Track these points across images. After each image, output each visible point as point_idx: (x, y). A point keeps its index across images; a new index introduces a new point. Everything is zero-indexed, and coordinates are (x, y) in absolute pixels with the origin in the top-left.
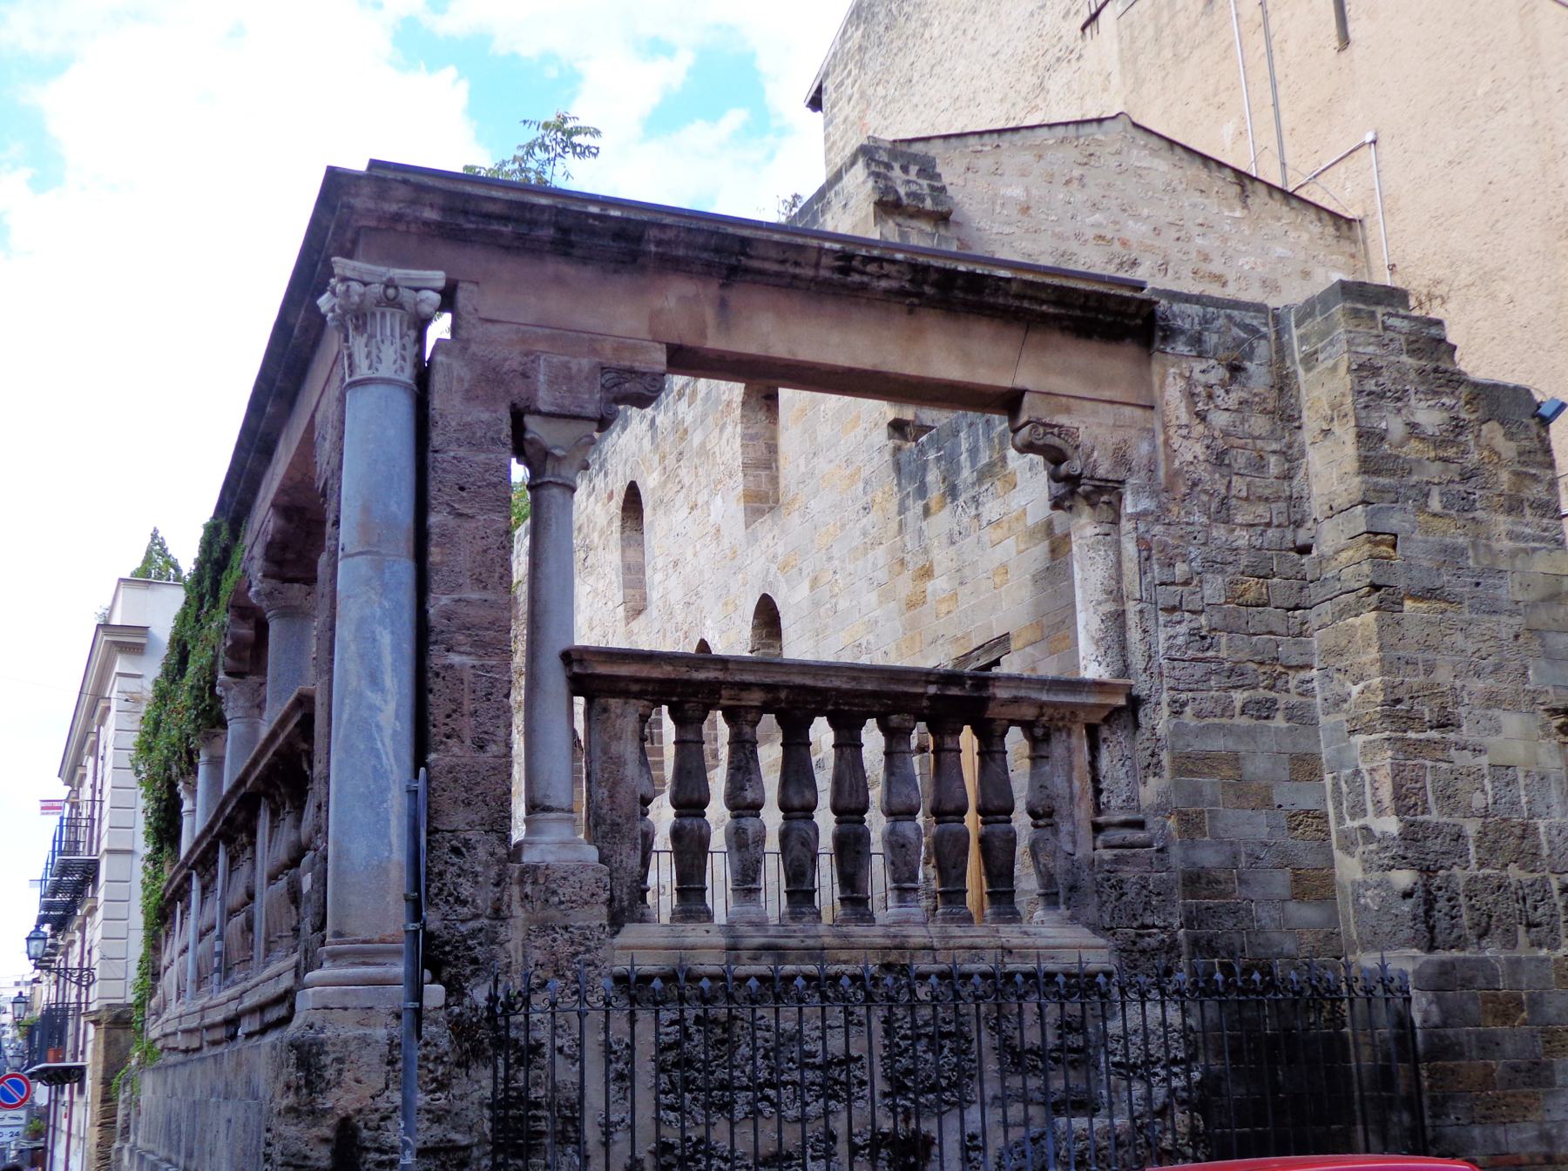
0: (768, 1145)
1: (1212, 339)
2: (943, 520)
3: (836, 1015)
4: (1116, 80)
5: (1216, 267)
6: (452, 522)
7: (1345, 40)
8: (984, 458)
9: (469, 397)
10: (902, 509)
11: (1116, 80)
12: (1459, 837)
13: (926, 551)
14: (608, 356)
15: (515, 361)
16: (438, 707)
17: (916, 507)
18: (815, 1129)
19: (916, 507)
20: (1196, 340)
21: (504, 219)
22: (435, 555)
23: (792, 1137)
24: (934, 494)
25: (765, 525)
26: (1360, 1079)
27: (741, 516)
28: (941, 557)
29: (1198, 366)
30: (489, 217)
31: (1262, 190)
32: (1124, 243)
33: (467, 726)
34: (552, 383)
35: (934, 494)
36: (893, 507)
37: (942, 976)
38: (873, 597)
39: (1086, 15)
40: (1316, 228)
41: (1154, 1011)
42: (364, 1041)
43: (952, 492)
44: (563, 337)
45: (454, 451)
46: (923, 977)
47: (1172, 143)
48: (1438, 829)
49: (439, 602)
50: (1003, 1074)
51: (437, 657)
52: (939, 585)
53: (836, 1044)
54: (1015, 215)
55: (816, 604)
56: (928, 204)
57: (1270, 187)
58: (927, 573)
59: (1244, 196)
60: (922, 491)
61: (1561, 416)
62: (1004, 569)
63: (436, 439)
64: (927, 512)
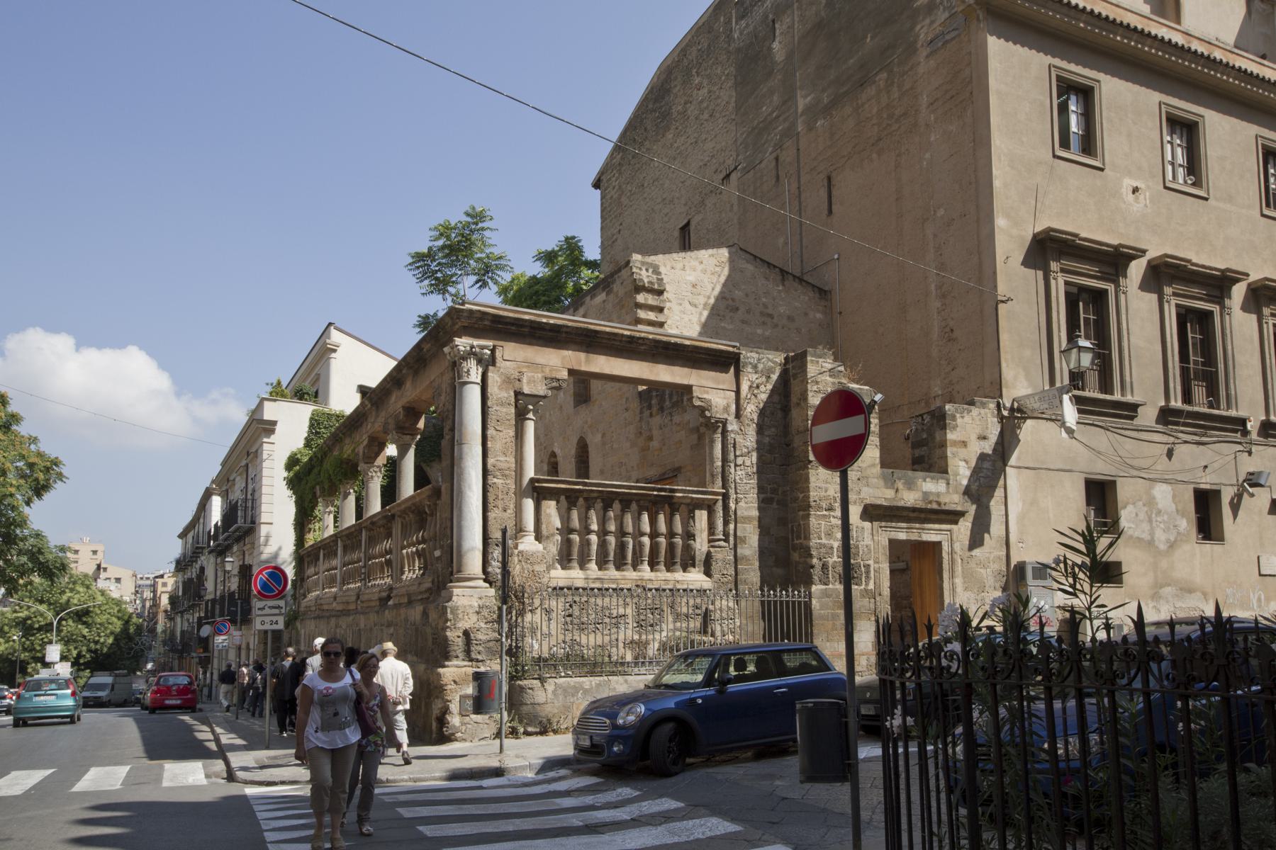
0: (599, 642)
1: (760, 366)
2: (657, 420)
3: (621, 602)
4: (735, 208)
5: (770, 311)
6: (494, 432)
7: (830, 212)
8: (675, 399)
9: (500, 388)
10: (641, 412)
11: (735, 208)
12: (832, 548)
13: (650, 430)
14: (547, 373)
15: (516, 375)
16: (491, 497)
17: (647, 413)
18: (614, 637)
19: (647, 413)
20: (755, 367)
21: (513, 324)
22: (489, 444)
23: (607, 639)
24: (655, 409)
25: (583, 410)
26: (1065, 720)
27: (572, 403)
28: (656, 433)
29: (755, 376)
30: (507, 324)
31: (791, 278)
32: (733, 300)
33: (500, 503)
34: (528, 383)
35: (655, 409)
36: (638, 411)
37: (657, 590)
38: (628, 444)
39: (724, 174)
40: (811, 294)
41: (724, 603)
42: (471, 606)
43: (662, 409)
44: (533, 365)
45: (495, 408)
46: (650, 590)
47: (755, 257)
48: (824, 546)
49: (490, 461)
50: (675, 622)
51: (491, 480)
52: (655, 444)
53: (621, 611)
54: (690, 288)
55: (604, 444)
56: (656, 287)
57: (794, 276)
58: (650, 438)
59: (783, 280)
60: (650, 407)
61: (497, 846)
62: (680, 442)
63: (489, 403)
64: (651, 415)
